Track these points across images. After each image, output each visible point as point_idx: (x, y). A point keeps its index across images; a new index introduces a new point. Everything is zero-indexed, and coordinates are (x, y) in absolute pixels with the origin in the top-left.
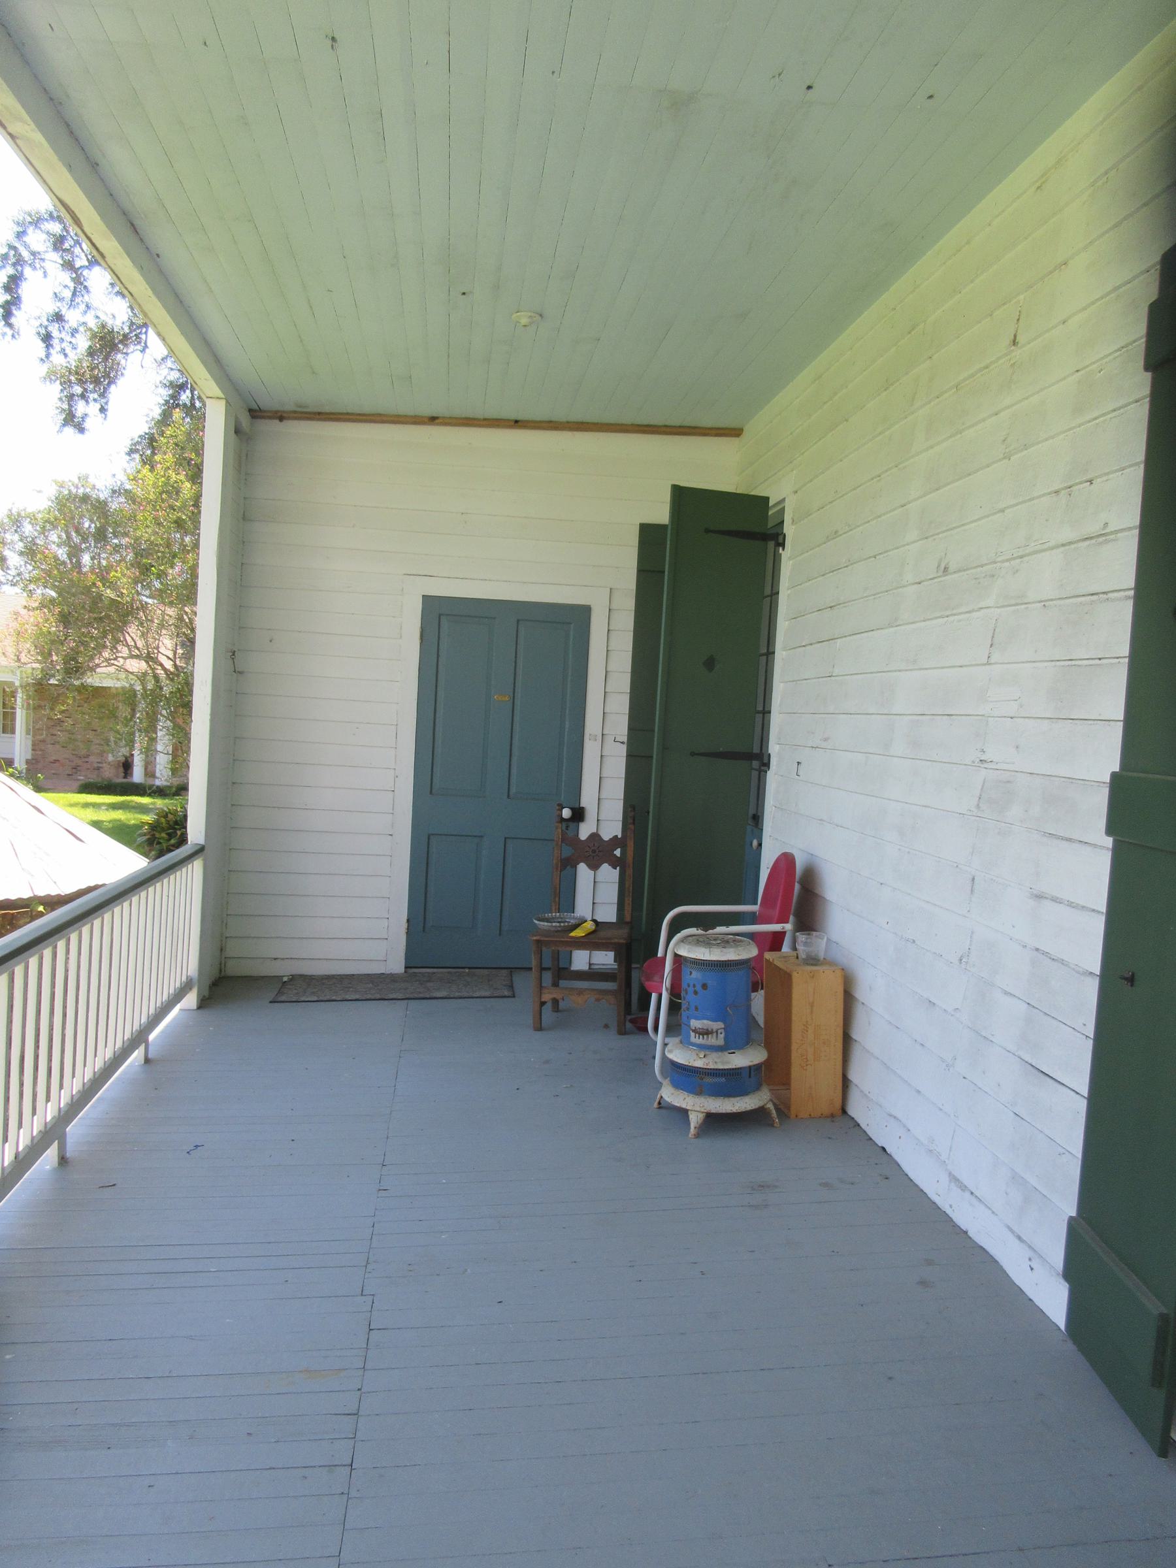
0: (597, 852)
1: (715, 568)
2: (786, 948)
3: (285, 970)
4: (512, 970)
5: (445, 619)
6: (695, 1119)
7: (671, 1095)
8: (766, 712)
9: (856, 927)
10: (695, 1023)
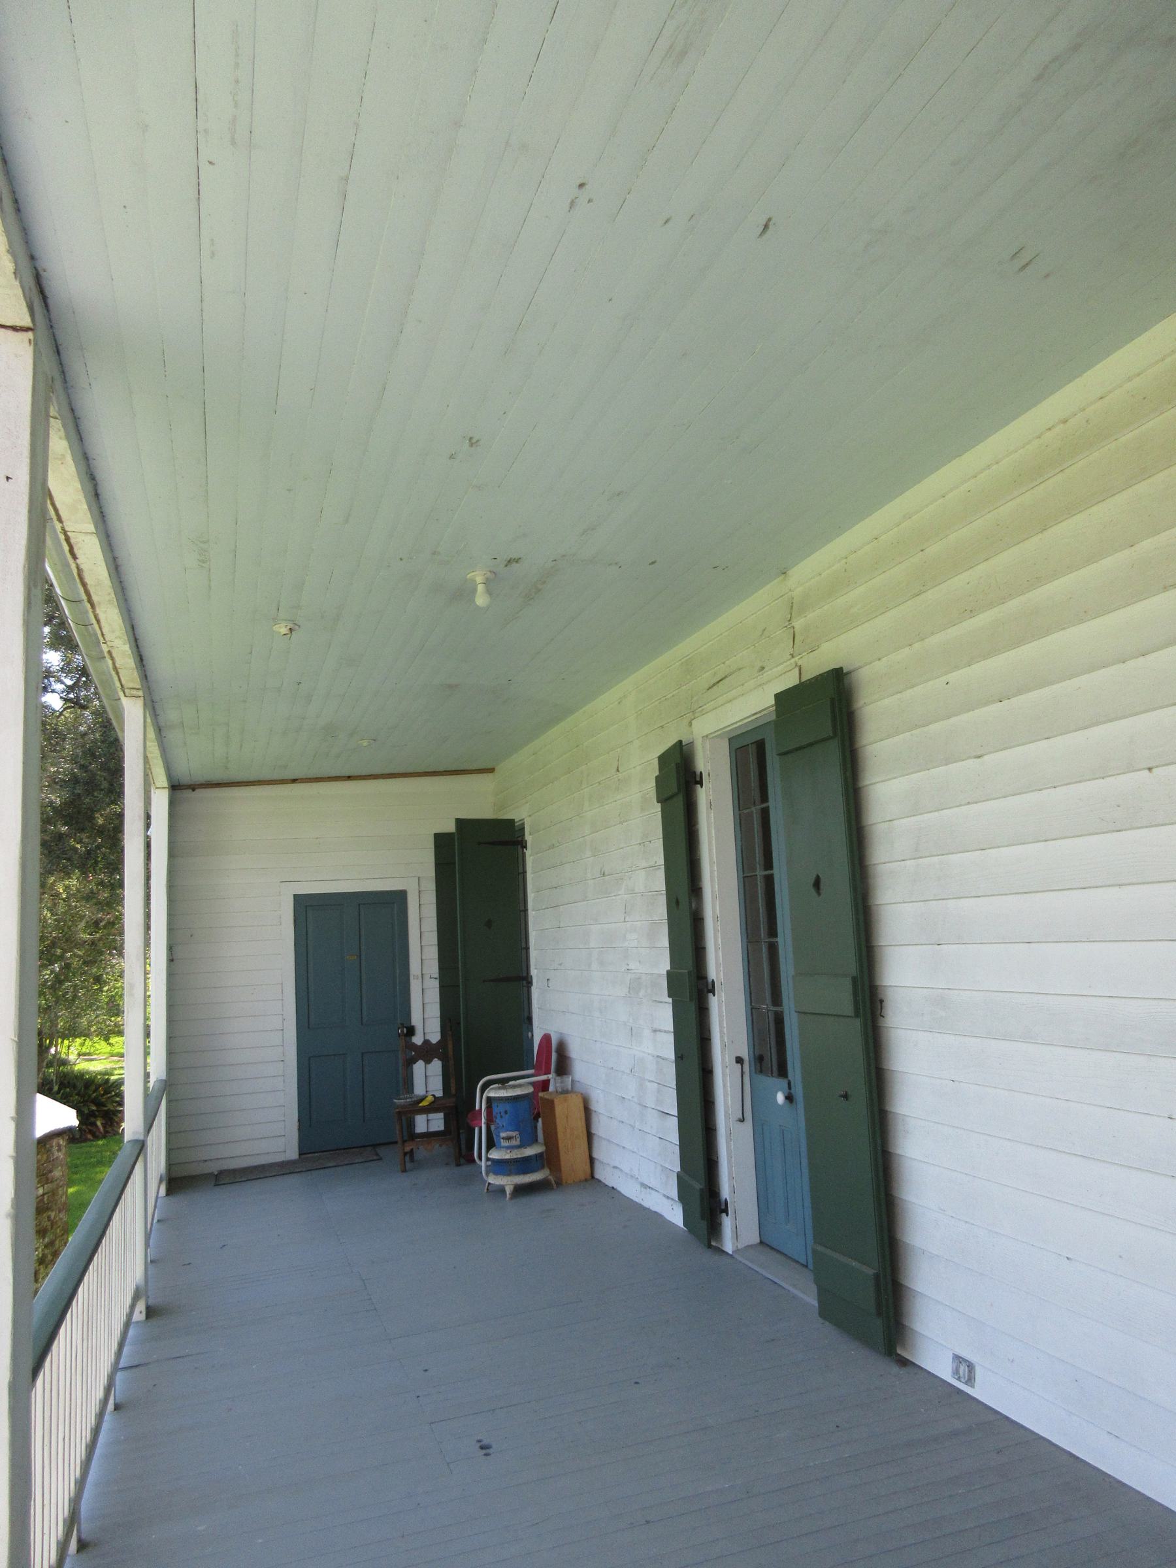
0: (427, 1052)
1: (484, 868)
2: (551, 1088)
3: (214, 1168)
4: (374, 1146)
5: (310, 911)
6: (509, 1190)
7: (495, 1180)
8: (527, 949)
9: (587, 1070)
10: (503, 1135)
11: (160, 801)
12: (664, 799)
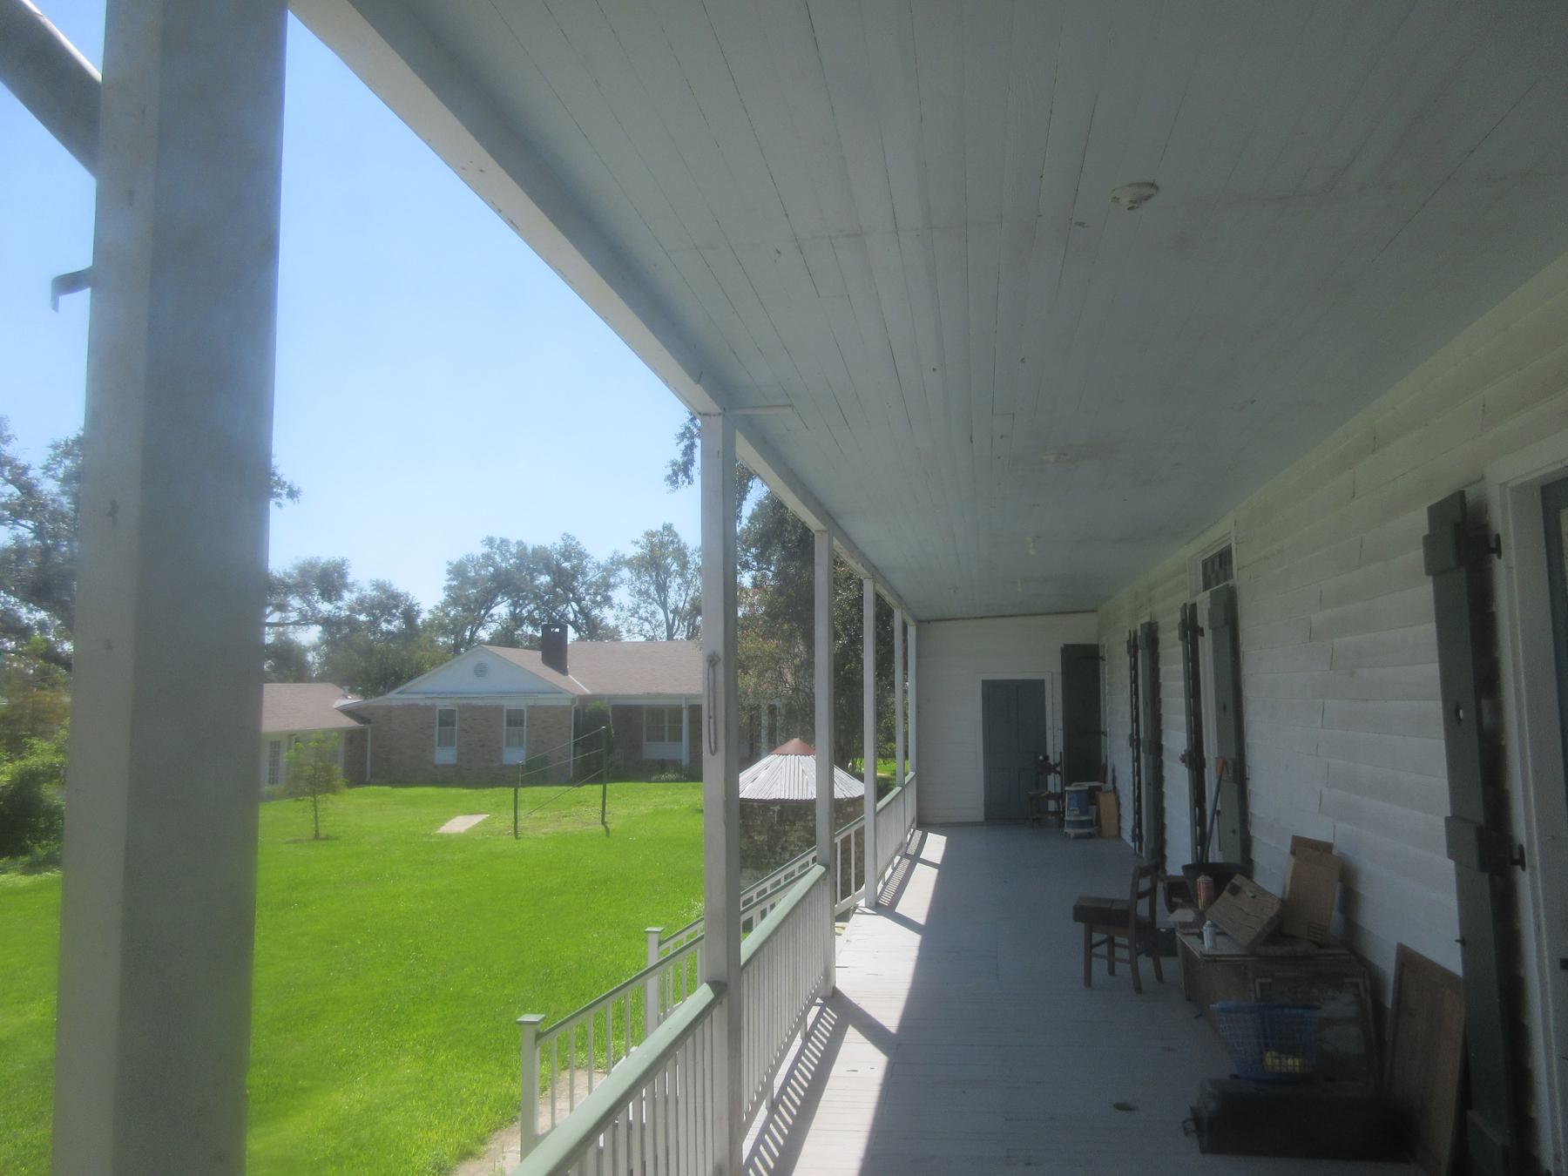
11: (912, 631)
12: (1435, 570)
